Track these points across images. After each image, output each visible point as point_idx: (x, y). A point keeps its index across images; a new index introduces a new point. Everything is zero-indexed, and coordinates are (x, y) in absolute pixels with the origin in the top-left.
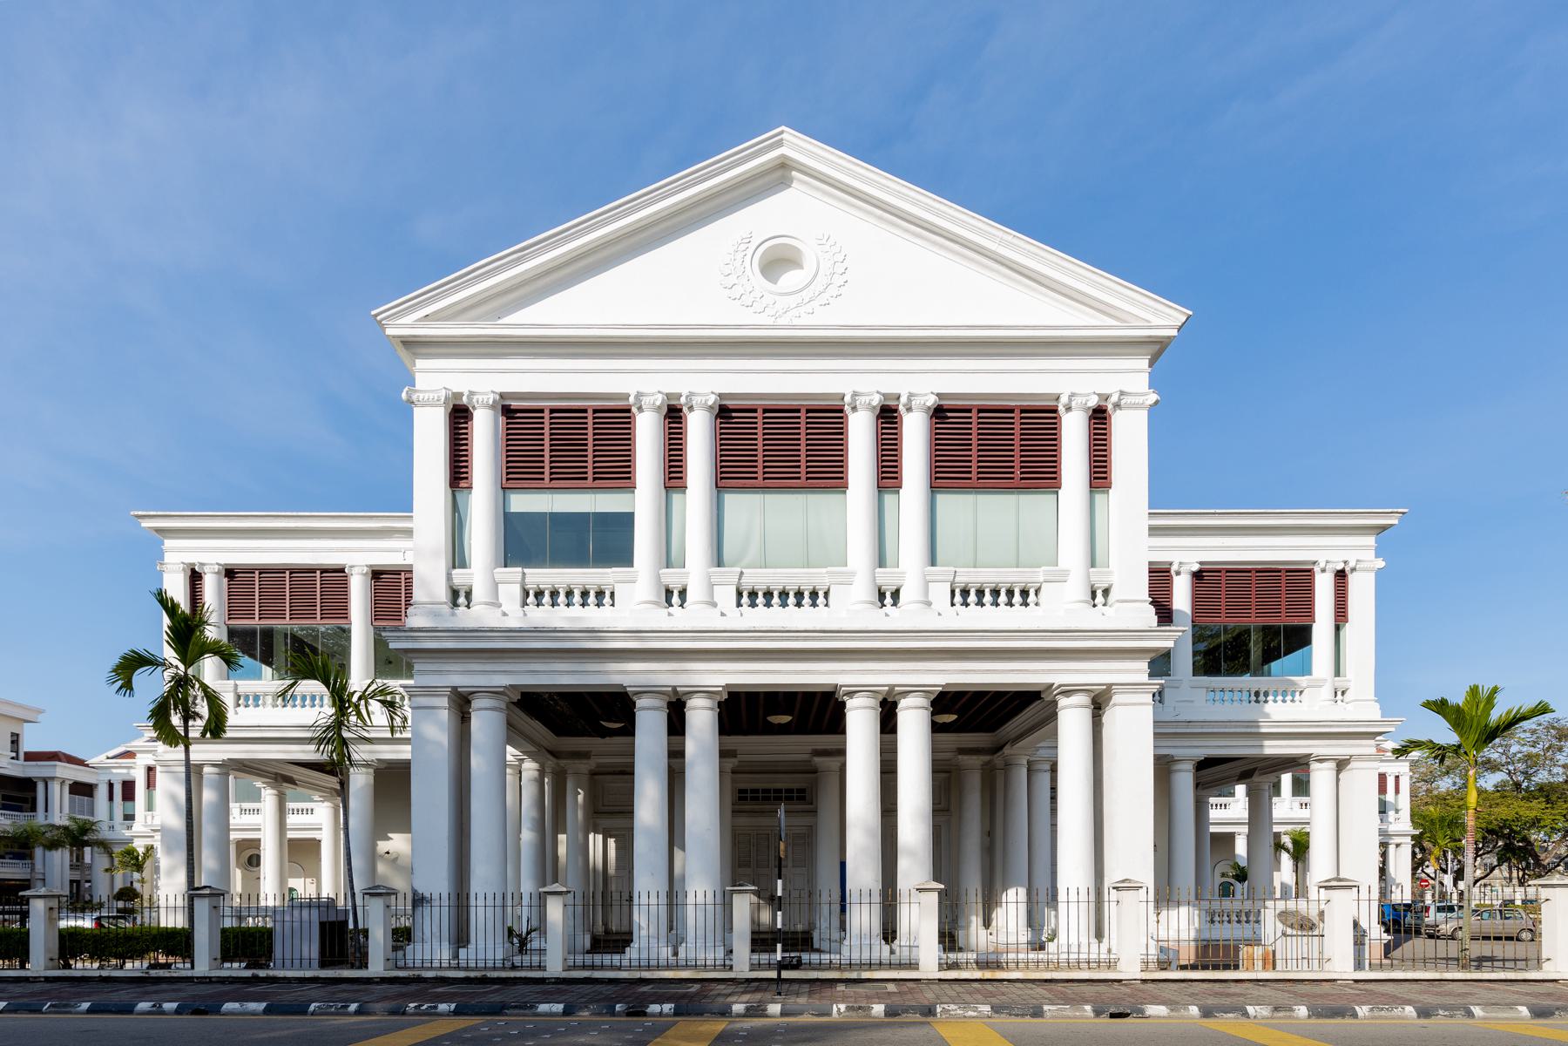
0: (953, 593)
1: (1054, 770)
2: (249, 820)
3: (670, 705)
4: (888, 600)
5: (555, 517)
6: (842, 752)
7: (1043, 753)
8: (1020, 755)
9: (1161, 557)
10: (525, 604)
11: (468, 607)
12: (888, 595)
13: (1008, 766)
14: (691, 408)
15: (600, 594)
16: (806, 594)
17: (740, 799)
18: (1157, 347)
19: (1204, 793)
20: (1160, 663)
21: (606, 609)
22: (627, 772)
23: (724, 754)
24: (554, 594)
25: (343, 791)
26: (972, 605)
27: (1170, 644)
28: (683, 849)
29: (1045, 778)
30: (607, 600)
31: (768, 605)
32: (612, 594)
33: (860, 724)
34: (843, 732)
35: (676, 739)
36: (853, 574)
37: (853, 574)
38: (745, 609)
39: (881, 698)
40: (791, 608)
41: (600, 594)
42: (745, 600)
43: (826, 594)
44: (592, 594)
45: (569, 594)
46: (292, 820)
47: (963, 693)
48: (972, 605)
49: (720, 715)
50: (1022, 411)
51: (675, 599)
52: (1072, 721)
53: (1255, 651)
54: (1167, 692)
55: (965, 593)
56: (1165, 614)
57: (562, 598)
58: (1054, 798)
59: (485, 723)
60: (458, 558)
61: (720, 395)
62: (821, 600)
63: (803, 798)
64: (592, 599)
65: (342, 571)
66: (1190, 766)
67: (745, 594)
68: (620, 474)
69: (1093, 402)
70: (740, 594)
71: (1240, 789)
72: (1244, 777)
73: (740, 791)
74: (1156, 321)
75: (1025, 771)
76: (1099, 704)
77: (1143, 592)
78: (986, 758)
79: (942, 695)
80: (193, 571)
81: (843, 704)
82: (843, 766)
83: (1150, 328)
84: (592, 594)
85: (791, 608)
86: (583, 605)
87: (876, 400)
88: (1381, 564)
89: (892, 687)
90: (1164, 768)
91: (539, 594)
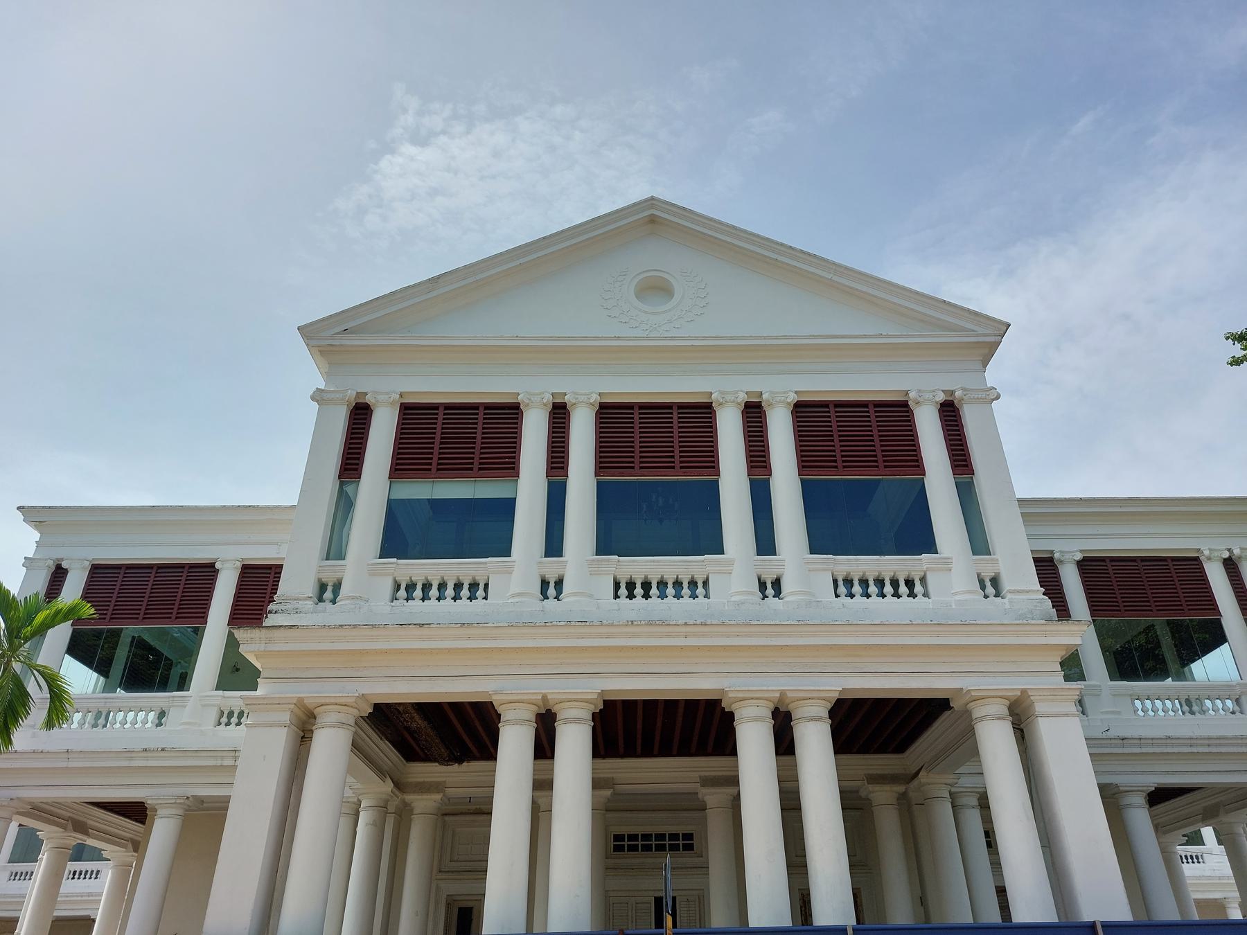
0: (835, 582)
1: (984, 804)
4: (770, 591)
6: (734, 781)
8: (936, 784)
9: (1044, 545)
10: (395, 598)
12: (769, 586)
15: (474, 586)
17: (618, 848)
18: (986, 351)
21: (479, 602)
22: (482, 811)
23: (597, 784)
25: (138, 846)
26: (889, 596)
27: (1078, 641)
28: (366, 394)
29: (973, 819)
30: (480, 593)
32: (486, 586)
33: (754, 740)
34: (733, 752)
36: (731, 563)
37: (731, 563)
38: (624, 601)
39: (772, 707)
40: (670, 600)
42: (623, 591)
43: (706, 583)
44: (466, 587)
45: (442, 586)
51: (552, 591)
55: (631, 586)
56: (1062, 610)
59: (330, 747)
60: (335, 549)
63: (689, 847)
64: (465, 592)
66: (1140, 800)
67: (623, 586)
68: (508, 465)
69: (941, 397)
70: (617, 586)
71: (1208, 833)
72: (1209, 815)
73: (618, 838)
74: (980, 330)
77: (1034, 584)
81: (730, 717)
82: (736, 802)
83: (977, 336)
84: (466, 587)
85: (670, 600)
87: (743, 398)
88: (88, 610)
89: (783, 693)
90: (1111, 797)
91: (411, 587)
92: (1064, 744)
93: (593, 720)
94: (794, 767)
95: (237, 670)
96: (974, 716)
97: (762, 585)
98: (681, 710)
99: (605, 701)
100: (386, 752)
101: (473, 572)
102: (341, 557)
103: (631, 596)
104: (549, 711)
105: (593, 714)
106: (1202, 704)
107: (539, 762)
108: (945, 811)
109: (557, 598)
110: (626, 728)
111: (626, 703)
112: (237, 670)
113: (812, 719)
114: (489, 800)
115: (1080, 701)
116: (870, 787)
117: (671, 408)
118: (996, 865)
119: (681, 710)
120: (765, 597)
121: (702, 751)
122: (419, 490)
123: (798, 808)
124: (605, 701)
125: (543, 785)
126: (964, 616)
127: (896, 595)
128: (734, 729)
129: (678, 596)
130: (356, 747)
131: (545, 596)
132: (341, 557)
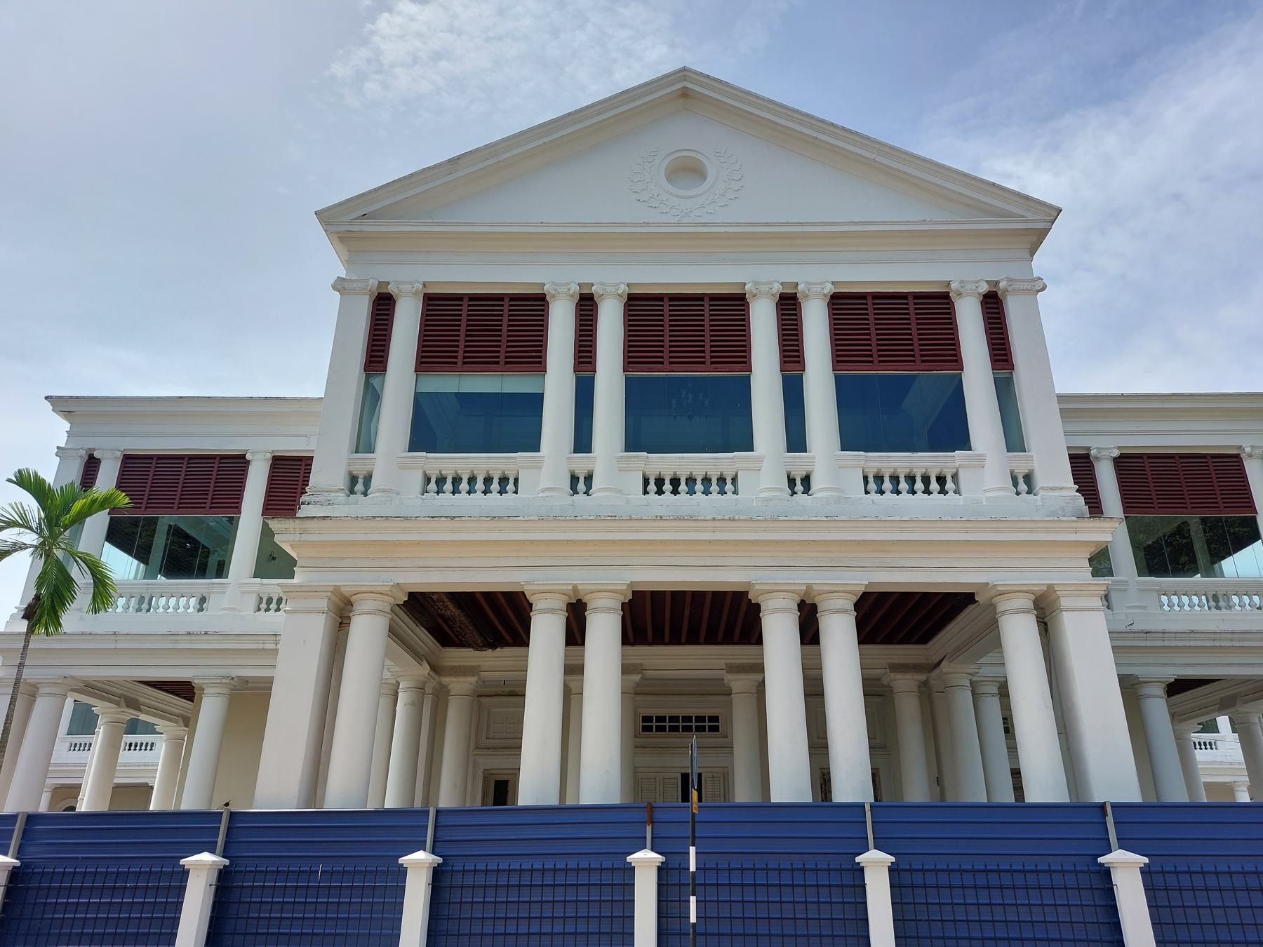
0: (866, 479)
1: (1004, 692)
2: (76, 756)
3: (802, 605)
4: (799, 488)
5: (463, 398)
6: (759, 668)
7: (987, 671)
8: (958, 674)
9: (1081, 442)
10: (425, 491)
11: (516, 492)
12: (798, 482)
14: (806, 296)
15: (504, 481)
16: (714, 482)
17: (646, 729)
19: (1183, 726)
20: (1100, 562)
21: (510, 496)
22: (516, 692)
23: (626, 669)
24: (457, 481)
27: (1108, 538)
29: (992, 707)
30: (510, 487)
31: (706, 492)
32: (516, 480)
33: (779, 630)
34: (759, 641)
36: (760, 459)
37: (760, 459)
39: (798, 599)
40: (699, 496)
43: (734, 480)
44: (496, 481)
45: (472, 480)
46: (125, 757)
47: (926, 596)
49: (623, 618)
50: (511, 299)
51: (581, 486)
52: (1019, 635)
53: (1199, 547)
54: (1113, 595)
55: (660, 482)
56: (1095, 506)
57: (464, 486)
58: (1009, 729)
59: (367, 633)
60: (364, 442)
61: (629, 285)
62: (729, 487)
63: (715, 729)
64: (495, 486)
65: (243, 456)
66: (1159, 691)
67: (652, 482)
68: (535, 359)
69: (984, 288)
70: (646, 482)
72: (1225, 705)
73: (646, 719)
74: (1030, 216)
75: (967, 695)
76: (1045, 614)
77: (1069, 482)
78: (923, 677)
79: (865, 596)
80: (91, 457)
84: (496, 481)
85: (699, 496)
86: (501, 493)
89: (809, 586)
90: (1130, 688)
91: (441, 481)
94: (819, 656)
95: (274, 559)
97: (791, 482)
99: (634, 592)
100: (422, 637)
101: (503, 467)
102: (803, 449)
104: (579, 601)
109: (587, 493)
110: (656, 618)
112: (274, 559)
116: (893, 675)
120: (794, 493)
123: (821, 694)
124: (634, 592)
125: (574, 670)
126: (994, 514)
130: (393, 632)
132: (803, 449)
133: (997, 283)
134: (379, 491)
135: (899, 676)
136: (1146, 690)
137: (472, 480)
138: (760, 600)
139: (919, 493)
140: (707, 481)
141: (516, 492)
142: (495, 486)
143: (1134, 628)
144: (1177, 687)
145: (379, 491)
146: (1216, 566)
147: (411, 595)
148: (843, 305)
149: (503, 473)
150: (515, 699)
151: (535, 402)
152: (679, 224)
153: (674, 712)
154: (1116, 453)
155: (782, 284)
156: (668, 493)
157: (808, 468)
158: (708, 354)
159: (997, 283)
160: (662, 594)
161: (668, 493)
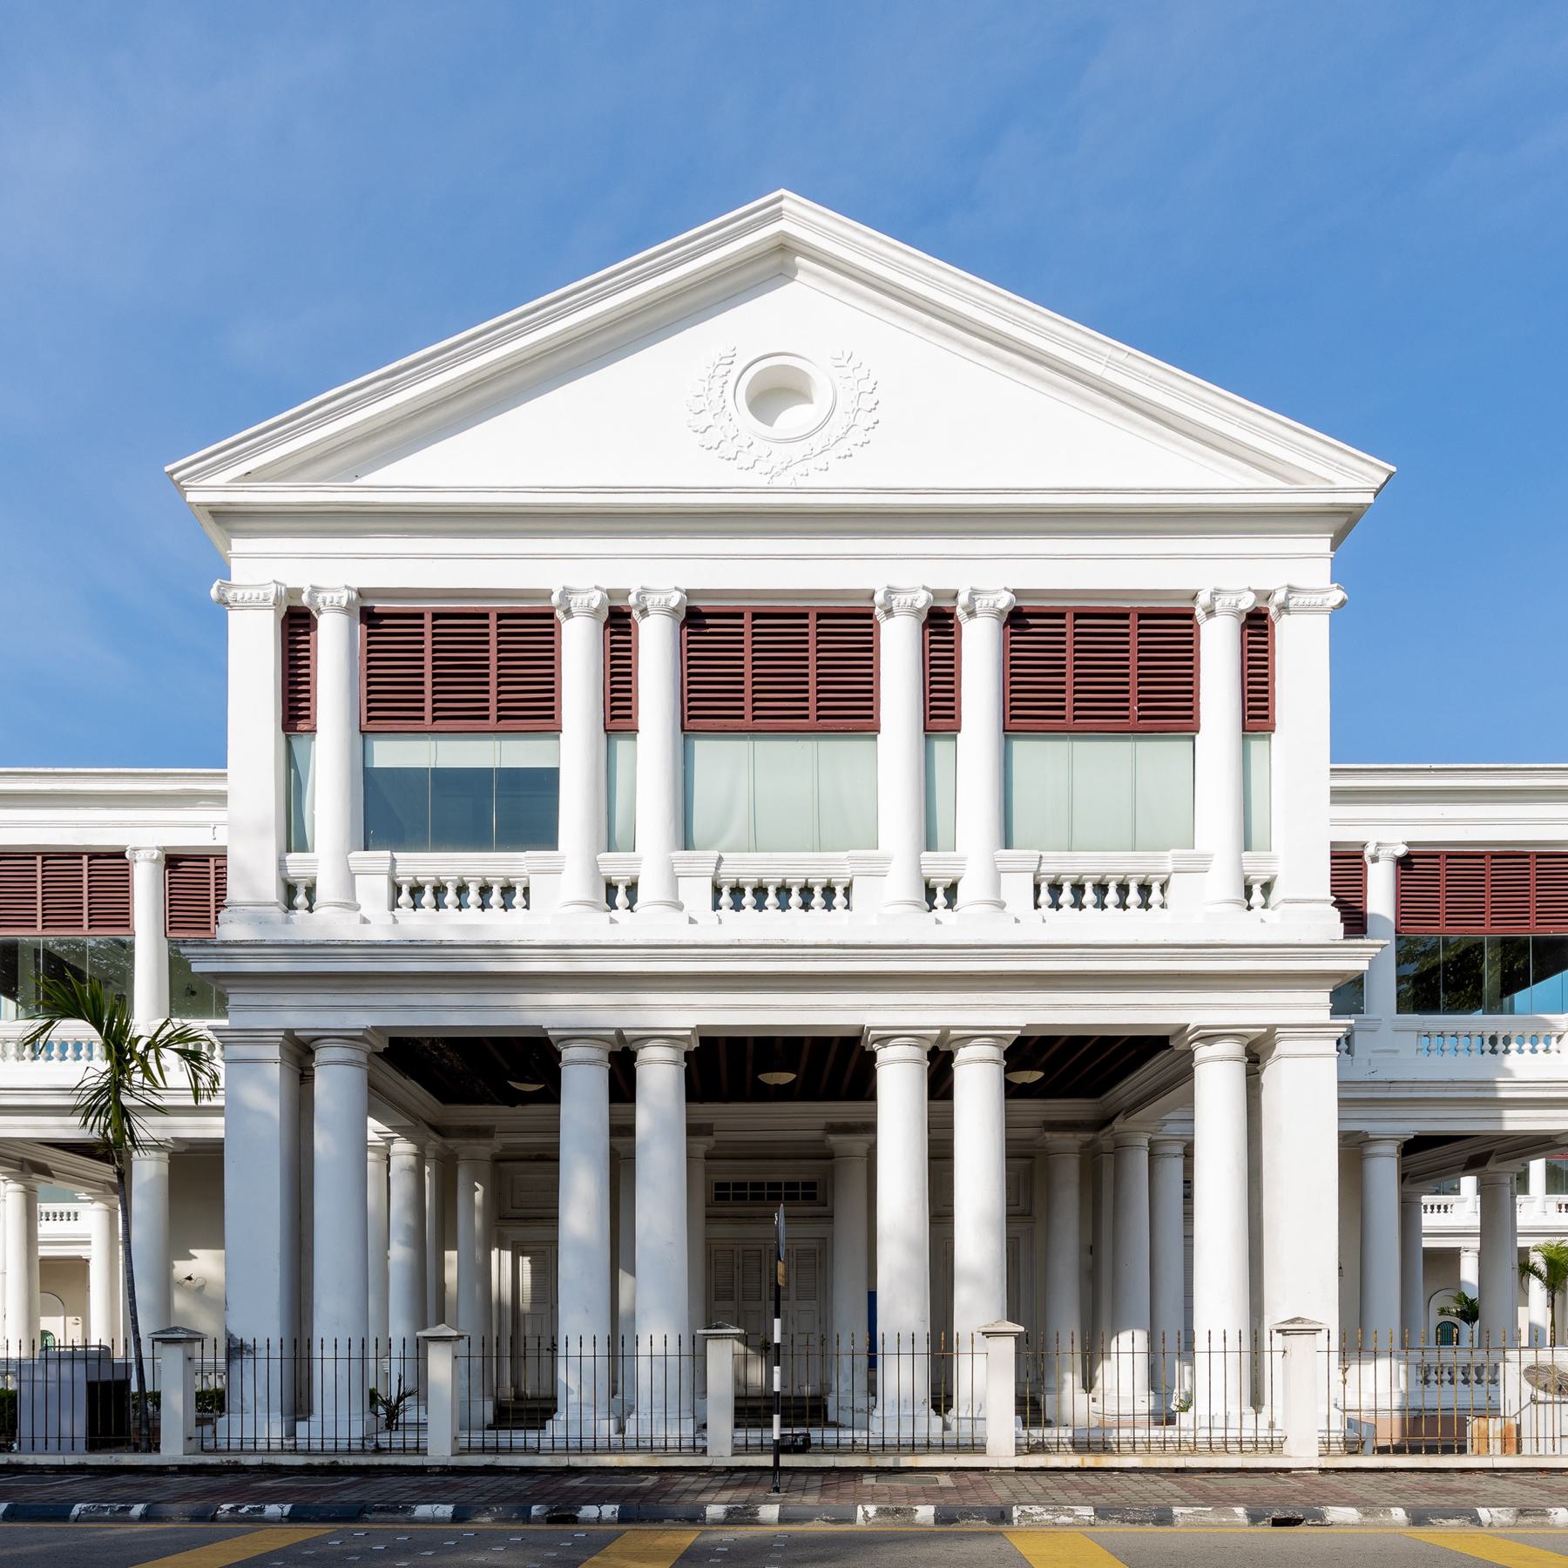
0: (1037, 888)
1: (1188, 1154)
3: (613, 1056)
4: (940, 899)
6: (870, 1128)
7: (1172, 1129)
8: (1138, 1131)
10: (395, 905)
11: (527, 907)
13: (1120, 1148)
15: (508, 891)
16: (818, 891)
17: (718, 1197)
18: (1343, 521)
21: (517, 913)
22: (550, 1157)
24: (439, 890)
25: (122, 1186)
26: (1066, 907)
29: (1175, 1167)
30: (518, 899)
32: (526, 891)
35: (940, 1104)
36: (887, 860)
37: (887, 860)
39: (929, 1046)
41: (508, 891)
43: (847, 891)
44: (496, 891)
45: (462, 890)
48: (1133, 908)
49: (688, 1072)
50: (1142, 616)
51: (621, 898)
53: (1490, 976)
56: (1355, 921)
57: (451, 897)
58: (1188, 1197)
59: (335, 1084)
60: (295, 836)
64: (495, 898)
65: (121, 855)
66: (1392, 1149)
67: (726, 891)
68: (536, 709)
70: (717, 891)
72: (1474, 1164)
73: (719, 1186)
74: (1341, 481)
77: (1324, 889)
78: (1089, 1136)
79: (1020, 1041)
83: (1333, 491)
84: (496, 891)
85: (795, 911)
87: (922, 600)
90: (1354, 1150)
91: (416, 891)
92: (1307, 1093)
93: (1006, 1058)
94: (950, 1114)
95: (193, 993)
96: (1197, 1058)
97: (930, 893)
98: (834, 1048)
99: (702, 1039)
100: (413, 1091)
101: (505, 871)
103: (737, 906)
104: (626, 1049)
105: (687, 1054)
106: (1547, 1043)
107: (615, 1105)
108: (1140, 1161)
109: (630, 908)
110: (719, 1066)
111: (731, 1041)
112: (193, 993)
113: (893, 1062)
114: (556, 1147)
115: (1348, 1039)
116: (1048, 1135)
117: (1125, 616)
118: (1188, 1215)
119: (834, 1048)
120: (933, 907)
121: (832, 1095)
122: (392, 753)
123: (949, 1157)
124: (702, 1039)
125: (622, 1131)
127: (1078, 904)
128: (875, 1071)
129: (760, 906)
130: (373, 1086)
131: (290, 906)
133: (1268, 596)
134: (329, 905)
135: (1056, 1135)
136: (1167, 1149)
137: (485, 891)
138: (953, 1047)
139: (1133, 908)
140: (783, 891)
141: (527, 907)
142: (495, 898)
143: (1374, 1077)
144: (1413, 1146)
145: (329, 905)
146: (1507, 1000)
147: (392, 1040)
148: (374, 618)
149: (760, 881)
150: (944, 1162)
151: (546, 782)
152: (768, 491)
153: (775, 1178)
154: (1401, 851)
155: (1015, 592)
156: (749, 908)
157: (956, 873)
158: (812, 704)
159: (1268, 596)
160: (742, 1041)
161: (749, 908)
